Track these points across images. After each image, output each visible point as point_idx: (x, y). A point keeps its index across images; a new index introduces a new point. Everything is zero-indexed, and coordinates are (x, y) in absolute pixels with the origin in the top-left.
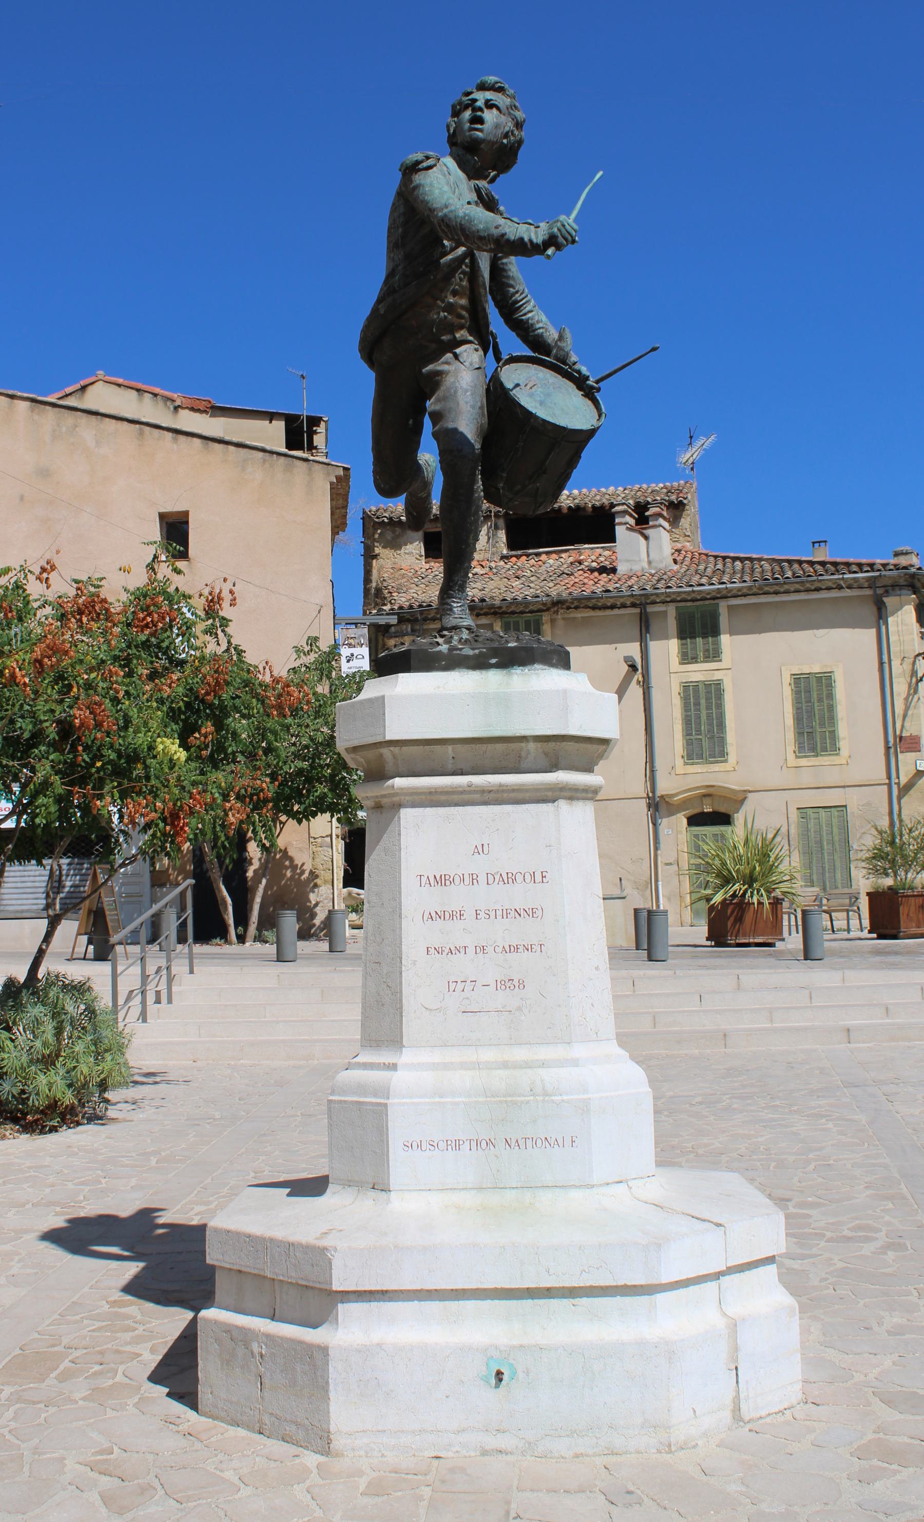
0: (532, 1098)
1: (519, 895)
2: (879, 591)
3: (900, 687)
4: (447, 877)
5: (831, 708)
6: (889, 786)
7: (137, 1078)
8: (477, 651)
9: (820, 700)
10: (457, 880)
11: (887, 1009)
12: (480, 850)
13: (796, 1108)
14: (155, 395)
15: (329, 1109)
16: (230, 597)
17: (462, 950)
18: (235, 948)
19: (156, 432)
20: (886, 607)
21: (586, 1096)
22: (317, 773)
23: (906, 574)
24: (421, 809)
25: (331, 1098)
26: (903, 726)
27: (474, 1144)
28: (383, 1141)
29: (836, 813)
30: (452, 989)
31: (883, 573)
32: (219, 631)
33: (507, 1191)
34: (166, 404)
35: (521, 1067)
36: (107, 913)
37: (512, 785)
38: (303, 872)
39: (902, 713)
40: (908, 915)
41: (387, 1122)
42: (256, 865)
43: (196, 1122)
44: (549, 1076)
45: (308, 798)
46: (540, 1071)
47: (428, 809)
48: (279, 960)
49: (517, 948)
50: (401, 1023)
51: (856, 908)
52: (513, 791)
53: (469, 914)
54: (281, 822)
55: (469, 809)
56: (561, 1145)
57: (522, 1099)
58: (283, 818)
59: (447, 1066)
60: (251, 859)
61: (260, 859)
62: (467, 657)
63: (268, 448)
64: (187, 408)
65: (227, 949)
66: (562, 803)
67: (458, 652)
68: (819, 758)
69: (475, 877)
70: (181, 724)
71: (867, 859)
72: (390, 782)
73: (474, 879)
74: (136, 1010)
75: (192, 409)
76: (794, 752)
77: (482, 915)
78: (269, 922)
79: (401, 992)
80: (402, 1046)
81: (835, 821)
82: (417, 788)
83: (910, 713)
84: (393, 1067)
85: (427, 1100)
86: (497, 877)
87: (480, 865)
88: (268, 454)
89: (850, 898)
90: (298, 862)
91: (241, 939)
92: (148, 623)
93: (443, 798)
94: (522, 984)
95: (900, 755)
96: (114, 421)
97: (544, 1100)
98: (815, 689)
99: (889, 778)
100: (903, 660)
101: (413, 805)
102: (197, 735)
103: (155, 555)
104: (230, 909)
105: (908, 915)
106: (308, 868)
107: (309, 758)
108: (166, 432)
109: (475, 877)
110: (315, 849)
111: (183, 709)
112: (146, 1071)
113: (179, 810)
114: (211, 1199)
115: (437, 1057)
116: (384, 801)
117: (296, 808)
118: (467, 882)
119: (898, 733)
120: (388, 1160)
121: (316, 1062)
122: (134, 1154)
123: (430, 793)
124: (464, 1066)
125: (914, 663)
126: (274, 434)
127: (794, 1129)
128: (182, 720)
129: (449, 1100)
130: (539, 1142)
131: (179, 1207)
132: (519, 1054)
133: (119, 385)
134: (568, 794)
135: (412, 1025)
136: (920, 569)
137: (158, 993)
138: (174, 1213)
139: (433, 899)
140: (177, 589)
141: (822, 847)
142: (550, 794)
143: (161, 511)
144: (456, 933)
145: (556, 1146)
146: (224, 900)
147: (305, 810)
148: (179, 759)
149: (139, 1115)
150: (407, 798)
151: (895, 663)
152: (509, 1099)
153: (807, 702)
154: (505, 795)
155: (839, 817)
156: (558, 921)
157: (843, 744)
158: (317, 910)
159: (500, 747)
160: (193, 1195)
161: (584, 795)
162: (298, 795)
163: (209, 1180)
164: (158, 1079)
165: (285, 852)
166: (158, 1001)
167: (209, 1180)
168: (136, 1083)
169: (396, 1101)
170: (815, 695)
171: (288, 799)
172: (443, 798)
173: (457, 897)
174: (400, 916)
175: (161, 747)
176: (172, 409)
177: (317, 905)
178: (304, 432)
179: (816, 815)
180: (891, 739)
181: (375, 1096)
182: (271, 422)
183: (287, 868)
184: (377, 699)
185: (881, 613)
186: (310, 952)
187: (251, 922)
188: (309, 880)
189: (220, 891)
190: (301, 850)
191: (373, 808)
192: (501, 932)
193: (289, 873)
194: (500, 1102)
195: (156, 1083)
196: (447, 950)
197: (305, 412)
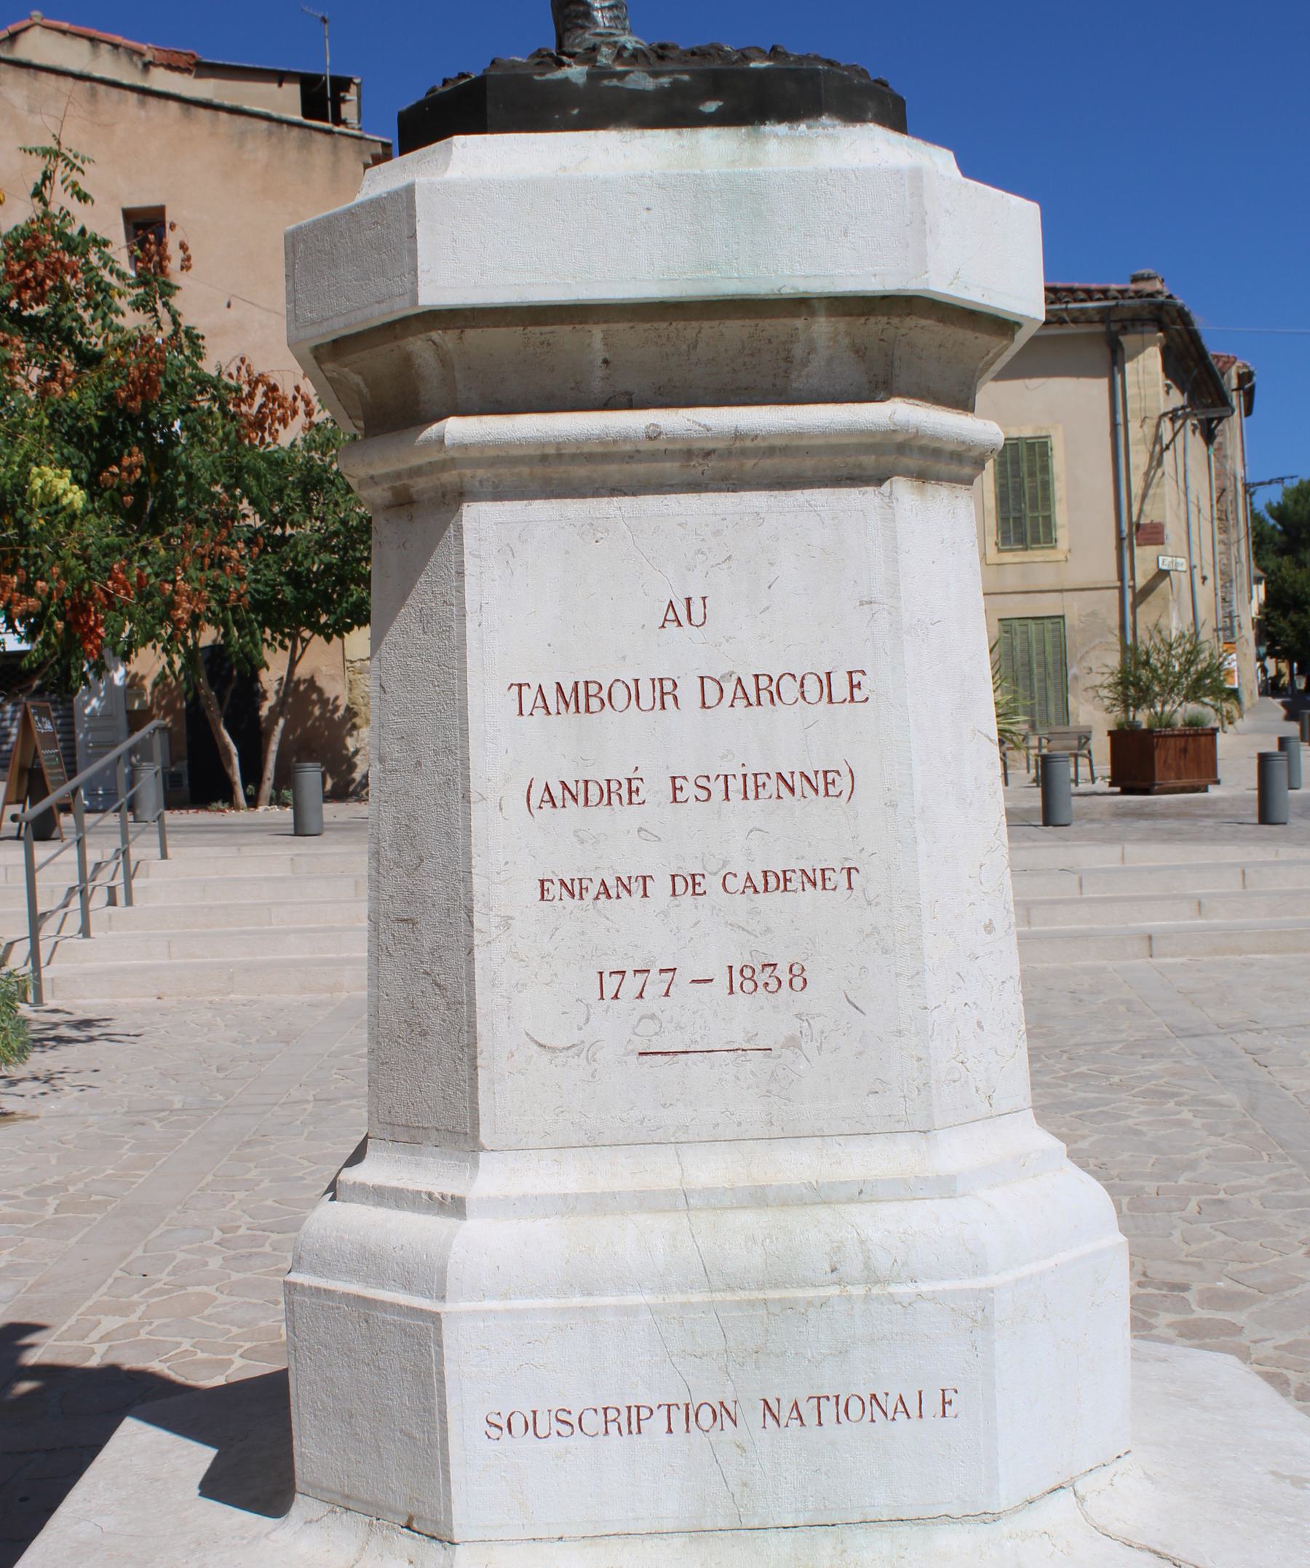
0: (834, 1291)
1: (786, 736)
2: (1115, 327)
3: (1139, 458)
4: (593, 689)
5: (1046, 486)
6: (1122, 590)
7: (65, 1032)
8: (665, 81)
9: (1032, 474)
10: (620, 695)
11: (1199, 904)
12: (679, 614)
13: (1116, 1079)
14: (116, 46)
15: (290, 1305)
16: (181, 254)
17: (637, 887)
18: (241, 816)
19: (115, 92)
20: (1123, 350)
21: (981, 1283)
22: (352, 570)
23: (1151, 304)
24: (518, 505)
25: (295, 1277)
26: (1141, 510)
27: (678, 1416)
28: (429, 1411)
29: (1050, 626)
30: (609, 991)
31: (1121, 302)
32: (159, 306)
33: (768, 1534)
34: (131, 60)
35: (802, 1202)
36: (47, 771)
37: (770, 435)
38: (336, 708)
39: (1140, 492)
40: (1165, 762)
41: (440, 1362)
42: (271, 701)
43: (141, 1118)
44: (877, 1226)
45: (340, 605)
46: (855, 1213)
47: (538, 504)
48: (297, 833)
49: (784, 880)
50: (474, 1088)
51: (1086, 752)
52: (771, 451)
53: (655, 789)
54: (303, 640)
55: (650, 504)
56: (914, 1411)
57: (810, 1293)
58: (306, 634)
59: (599, 1204)
60: (265, 692)
61: (277, 692)
62: (639, 96)
63: (275, 114)
64: (161, 65)
65: (231, 816)
66: (901, 487)
67: (615, 82)
68: (1030, 552)
69: (668, 686)
70: (93, 456)
71: (1110, 686)
72: (432, 431)
73: (665, 692)
74: (75, 921)
75: (170, 67)
76: (996, 544)
77: (689, 790)
78: (286, 778)
79: (472, 1003)
80: (477, 1148)
81: (1048, 636)
82: (509, 444)
83: (1151, 492)
84: (454, 1207)
85: (551, 1302)
86: (729, 688)
87: (683, 656)
88: (274, 124)
89: (1080, 738)
90: (330, 693)
91: (253, 802)
92: (28, 281)
93: (580, 472)
94: (799, 977)
95: (1137, 551)
96: (53, 77)
97: (867, 1298)
98: (1025, 458)
99: (1121, 577)
100: (1143, 420)
101: (498, 495)
102: (116, 470)
103: (45, 174)
104: (236, 761)
105: (1165, 762)
106: (343, 702)
107: (340, 549)
108: (129, 93)
109: (668, 686)
110: (352, 677)
111: (96, 429)
112: (80, 1015)
113: (87, 599)
114: (135, 1297)
115: (569, 1176)
116: (420, 484)
117: (323, 619)
118: (646, 700)
119: (1134, 519)
120: (446, 1464)
121: (345, 995)
122: (20, 1192)
123: (544, 459)
124: (647, 1201)
125: (1158, 425)
126: (287, 100)
127: (1130, 1122)
128: (95, 450)
129: (609, 1300)
130: (855, 1407)
131: (72, 1321)
132: (796, 1165)
133: (64, 32)
134: (912, 462)
135: (505, 1087)
136: (1170, 297)
137: (112, 890)
138: (61, 1338)
139: (557, 749)
140: (83, 232)
141: (1030, 671)
142: (869, 460)
143: (128, 205)
144: (617, 842)
145: (901, 1417)
146: (226, 748)
147: (336, 622)
148: (71, 503)
149: (52, 1105)
150: (481, 473)
151: (1134, 426)
152: (773, 1294)
153: (1014, 476)
154: (750, 463)
155: (1054, 631)
156: (894, 805)
157: (1062, 534)
158: (358, 759)
159: (735, 329)
160: (104, 1289)
161: (954, 468)
162: (327, 602)
163: (139, 1252)
164: (95, 1032)
165: (311, 682)
166: (112, 902)
167: (139, 1252)
168: (60, 1040)
169: (464, 1306)
170: (1024, 467)
171: (312, 608)
172: (580, 472)
173: (618, 743)
174: (466, 797)
175: (38, 483)
176: (140, 66)
177: (356, 752)
178: (326, 99)
179: (1023, 628)
180: (1125, 527)
181: (407, 1286)
182: (280, 85)
183: (314, 703)
184: (394, 196)
185: (1113, 361)
186: (346, 819)
187: (265, 779)
188: (344, 720)
189: (221, 736)
190: (333, 678)
191: (388, 507)
192: (743, 836)
193: (317, 711)
194: (751, 1303)
195: (91, 1039)
196: (595, 888)
197: (328, 69)
